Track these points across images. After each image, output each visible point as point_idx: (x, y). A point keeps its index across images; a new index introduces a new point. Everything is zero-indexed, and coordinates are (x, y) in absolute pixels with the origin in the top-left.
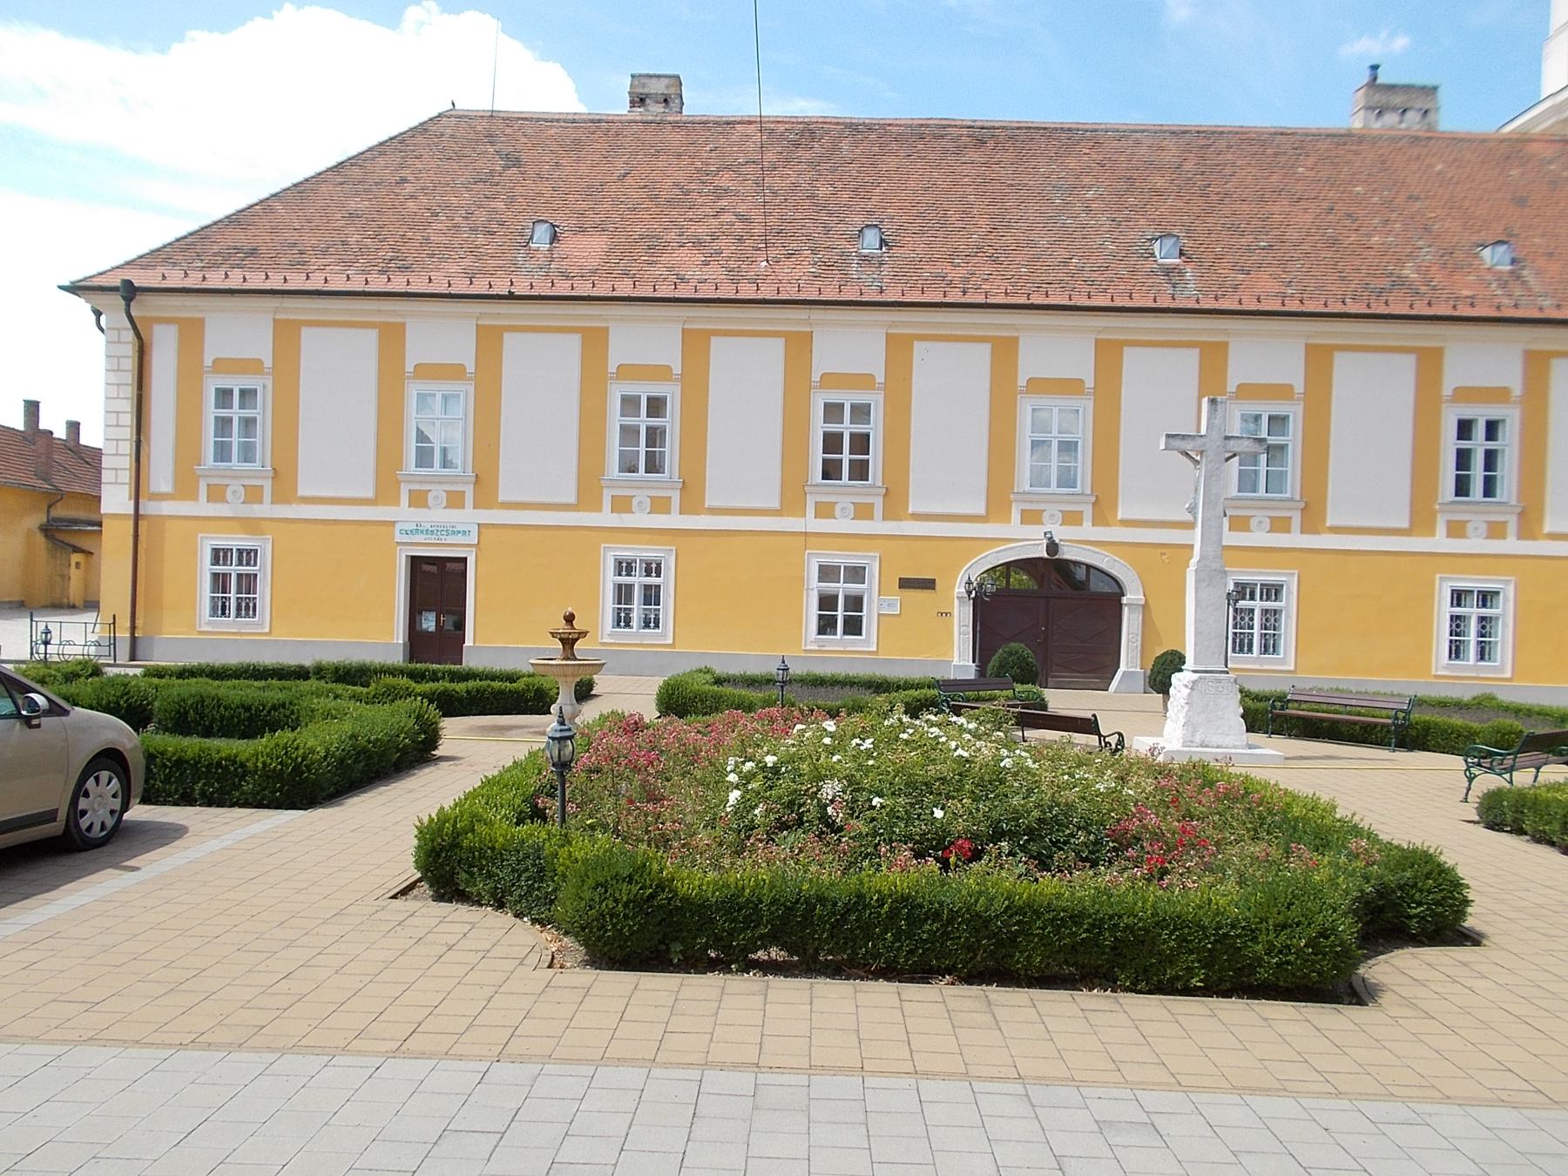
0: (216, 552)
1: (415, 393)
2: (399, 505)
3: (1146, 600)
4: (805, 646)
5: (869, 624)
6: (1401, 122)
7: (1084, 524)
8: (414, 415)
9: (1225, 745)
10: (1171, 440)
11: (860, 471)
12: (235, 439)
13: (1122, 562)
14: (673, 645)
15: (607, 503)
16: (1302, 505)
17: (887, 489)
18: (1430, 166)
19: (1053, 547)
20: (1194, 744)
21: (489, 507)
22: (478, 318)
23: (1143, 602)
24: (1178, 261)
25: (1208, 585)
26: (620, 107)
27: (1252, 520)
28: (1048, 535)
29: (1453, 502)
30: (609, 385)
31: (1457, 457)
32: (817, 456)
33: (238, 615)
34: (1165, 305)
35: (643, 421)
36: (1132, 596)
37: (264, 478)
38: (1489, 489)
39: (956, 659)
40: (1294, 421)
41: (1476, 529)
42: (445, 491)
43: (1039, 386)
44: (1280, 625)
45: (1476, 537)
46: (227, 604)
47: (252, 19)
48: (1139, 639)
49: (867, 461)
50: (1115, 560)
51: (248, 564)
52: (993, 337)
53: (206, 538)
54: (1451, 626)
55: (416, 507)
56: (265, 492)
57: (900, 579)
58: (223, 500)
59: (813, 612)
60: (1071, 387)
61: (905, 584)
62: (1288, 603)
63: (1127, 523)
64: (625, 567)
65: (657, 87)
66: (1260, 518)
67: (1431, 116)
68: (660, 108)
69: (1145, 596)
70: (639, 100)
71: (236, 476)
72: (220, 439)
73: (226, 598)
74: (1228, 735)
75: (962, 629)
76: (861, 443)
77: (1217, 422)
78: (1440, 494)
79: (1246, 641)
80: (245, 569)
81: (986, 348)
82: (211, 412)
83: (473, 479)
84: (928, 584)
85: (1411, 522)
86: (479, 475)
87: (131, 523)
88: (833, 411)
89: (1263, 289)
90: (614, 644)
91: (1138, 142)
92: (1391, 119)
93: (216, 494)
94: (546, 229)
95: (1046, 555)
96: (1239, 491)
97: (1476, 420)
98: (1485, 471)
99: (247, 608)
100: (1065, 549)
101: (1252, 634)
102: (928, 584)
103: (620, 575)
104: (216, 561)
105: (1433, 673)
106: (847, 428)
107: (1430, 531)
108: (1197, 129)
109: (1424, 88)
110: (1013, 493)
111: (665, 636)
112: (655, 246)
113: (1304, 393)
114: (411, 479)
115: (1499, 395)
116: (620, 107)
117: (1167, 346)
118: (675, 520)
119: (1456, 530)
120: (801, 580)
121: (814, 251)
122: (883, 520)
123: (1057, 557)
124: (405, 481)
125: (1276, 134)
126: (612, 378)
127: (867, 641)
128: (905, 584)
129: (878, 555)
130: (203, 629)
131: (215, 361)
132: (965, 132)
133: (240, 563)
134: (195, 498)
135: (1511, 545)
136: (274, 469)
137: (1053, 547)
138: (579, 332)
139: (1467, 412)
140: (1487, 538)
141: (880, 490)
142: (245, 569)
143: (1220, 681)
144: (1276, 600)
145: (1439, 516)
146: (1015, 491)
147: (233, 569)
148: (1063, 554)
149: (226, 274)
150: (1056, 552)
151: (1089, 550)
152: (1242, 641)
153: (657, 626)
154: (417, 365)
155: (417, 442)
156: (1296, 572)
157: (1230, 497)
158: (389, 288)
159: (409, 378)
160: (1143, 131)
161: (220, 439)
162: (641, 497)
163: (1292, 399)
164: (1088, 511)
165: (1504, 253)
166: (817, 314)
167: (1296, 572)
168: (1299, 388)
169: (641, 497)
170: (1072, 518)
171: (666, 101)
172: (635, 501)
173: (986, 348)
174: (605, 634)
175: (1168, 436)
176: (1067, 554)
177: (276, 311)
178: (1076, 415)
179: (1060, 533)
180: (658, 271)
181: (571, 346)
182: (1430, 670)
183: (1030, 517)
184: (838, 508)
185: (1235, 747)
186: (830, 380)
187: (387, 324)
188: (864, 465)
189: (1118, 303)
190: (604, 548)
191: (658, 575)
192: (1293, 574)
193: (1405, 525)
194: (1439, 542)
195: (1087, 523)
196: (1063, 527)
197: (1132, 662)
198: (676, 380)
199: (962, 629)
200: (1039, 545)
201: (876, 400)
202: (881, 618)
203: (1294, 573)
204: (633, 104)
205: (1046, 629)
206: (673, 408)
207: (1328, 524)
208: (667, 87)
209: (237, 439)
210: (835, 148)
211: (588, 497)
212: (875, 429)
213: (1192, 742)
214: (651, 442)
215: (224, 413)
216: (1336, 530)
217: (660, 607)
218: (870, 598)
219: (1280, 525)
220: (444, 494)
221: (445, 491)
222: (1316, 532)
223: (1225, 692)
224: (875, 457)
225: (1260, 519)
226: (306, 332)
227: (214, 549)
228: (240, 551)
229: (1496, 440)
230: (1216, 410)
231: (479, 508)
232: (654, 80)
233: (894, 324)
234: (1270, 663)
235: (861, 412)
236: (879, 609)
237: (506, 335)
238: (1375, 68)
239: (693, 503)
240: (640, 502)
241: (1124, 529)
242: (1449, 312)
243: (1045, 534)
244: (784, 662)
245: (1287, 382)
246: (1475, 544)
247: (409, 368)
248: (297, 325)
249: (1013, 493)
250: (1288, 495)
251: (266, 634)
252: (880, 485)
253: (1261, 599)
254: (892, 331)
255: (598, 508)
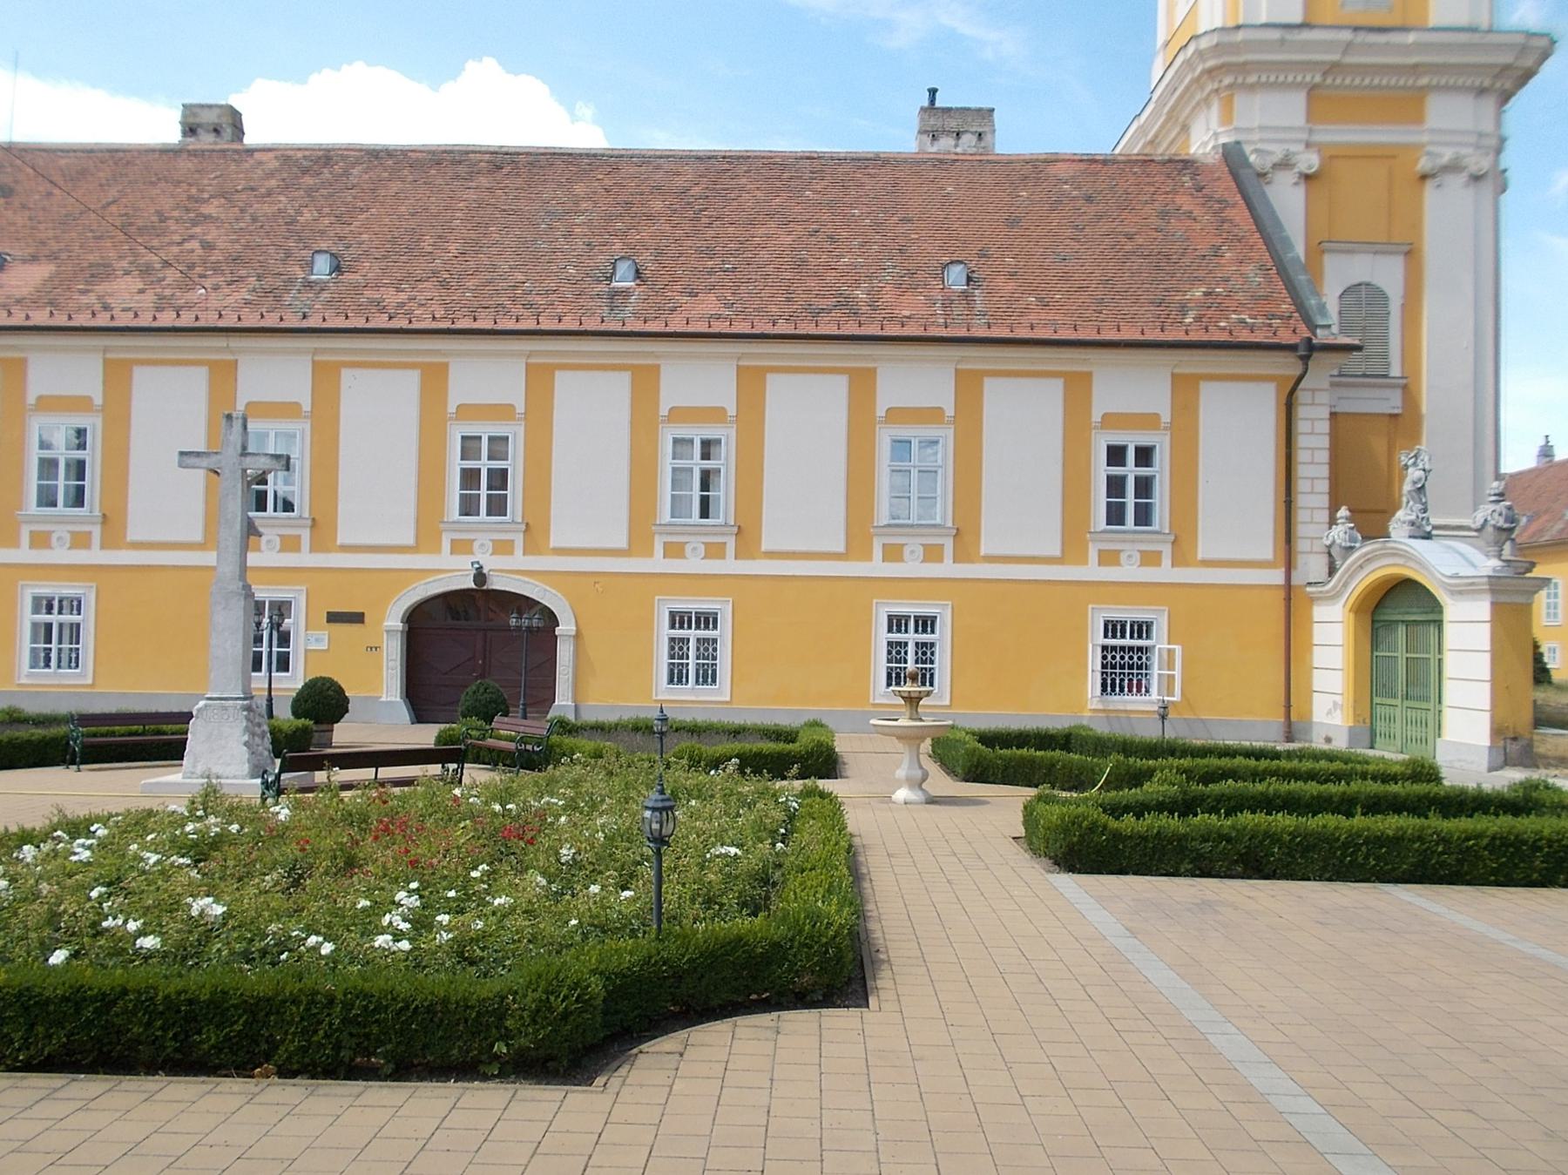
0: (37, 600)
1: (888, 440)
2: (1086, 563)
3: (578, 631)
4: (656, 695)
5: (297, 660)
6: (956, 146)
7: (945, 561)
8: (888, 462)
9: (225, 775)
10: (185, 458)
11: (498, 506)
12: (1130, 500)
13: (554, 591)
14: (92, 686)
15: (446, 546)
16: (1172, 538)
17: (958, 529)
18: (942, 188)
19: (480, 577)
20: (195, 776)
21: (971, 561)
22: (314, 354)
23: (574, 633)
24: (632, 283)
25: (224, 608)
26: (171, 135)
27: (1122, 554)
28: (476, 566)
29: (889, 526)
30: (877, 429)
31: (1064, 486)
32: (454, 491)
33: (697, 682)
34: (211, 324)
35: (1130, 470)
36: (565, 628)
37: (93, 523)
38: (1144, 516)
39: (384, 696)
40: (1161, 453)
41: (912, 552)
42: (923, 545)
43: (897, 415)
44: (1152, 664)
45: (913, 560)
46: (684, 671)
47: (350, 63)
48: (571, 670)
49: (84, 486)
50: (545, 590)
51: (899, 631)
52: (423, 363)
53: (27, 585)
54: (688, 649)
55: (1105, 565)
56: (302, 542)
57: (328, 613)
58: (1117, 563)
59: (25, 644)
60: (932, 415)
61: (334, 618)
62: (723, 632)
63: (771, 555)
64: (897, 623)
65: (209, 118)
66: (696, 544)
67: (987, 138)
68: (211, 138)
69: (577, 625)
70: (190, 130)
71: (61, 521)
72: (46, 482)
73: (682, 664)
74: (229, 765)
75: (390, 664)
76: (499, 479)
77: (231, 438)
78: (1092, 525)
79: (1109, 682)
80: (703, 633)
81: (626, 377)
82: (1101, 471)
83: (100, 520)
84: (357, 618)
85: (1063, 551)
86: (317, 518)
87: (1282, 594)
88: (469, 446)
89: (702, 311)
90: (32, 685)
91: (658, 167)
92: (946, 143)
93: (893, 554)
94: (629, 266)
95: (474, 587)
96: (672, 517)
97: (1155, 446)
98: (702, 491)
99: (707, 676)
100: (495, 579)
101: (50, 649)
102: (357, 618)
103: (71, 614)
104: (36, 610)
105: (871, 701)
106: (484, 464)
107: (1082, 560)
108: (723, 154)
109: (979, 110)
110: (1090, 532)
111: (941, 697)
112: (102, 272)
113: (525, 414)
114: (32, 520)
115: (1149, 421)
116: (171, 135)
117: (181, 364)
118: (96, 556)
119: (1108, 558)
120: (648, 624)
121: (259, 277)
122: (311, 552)
123: (485, 588)
124: (660, 534)
125: (802, 158)
126: (663, 422)
127: (293, 678)
128: (334, 618)
129: (304, 588)
130: (877, 701)
131: (1105, 416)
132: (487, 157)
133: (698, 627)
134: (650, 554)
135: (730, 565)
136: (314, 519)
137: (480, 577)
138: (1061, 377)
139: (1117, 439)
140: (1141, 565)
141: (304, 521)
142: (703, 633)
143: (225, 708)
144: (1147, 638)
145: (875, 540)
146: (875, 524)
147: (693, 634)
148: (492, 584)
149: (51, 312)
150: (484, 583)
151: (519, 580)
152: (680, 672)
153: (714, 681)
154: (889, 409)
155: (40, 478)
156: (950, 603)
157: (451, 520)
158: (178, 324)
159: (451, 419)
160: (669, 157)
161: (46, 482)
162: (61, 532)
163: (514, 419)
164: (519, 539)
165: (960, 272)
166: (236, 342)
167: (950, 603)
168: (1166, 417)
169: (61, 532)
170: (503, 548)
171: (216, 130)
172: (54, 537)
173: (626, 377)
174: (22, 676)
175: (182, 453)
176: (497, 583)
177: (106, 350)
178: (45, 437)
179: (490, 563)
180: (91, 299)
181: (410, 381)
182: (869, 699)
183: (460, 547)
184: (907, 550)
185: (235, 777)
186: (466, 412)
187: (430, 364)
188: (80, 491)
189: (545, 326)
190: (22, 586)
191: (715, 627)
192: (92, 587)
193: (841, 548)
194: (1092, 571)
195: (519, 551)
196: (493, 557)
197: (563, 695)
198: (1165, 429)
199: (390, 664)
200: (467, 575)
201: (516, 433)
202: (309, 654)
203: (1164, 610)
204: (185, 134)
205: (484, 662)
206: (1162, 459)
207: (763, 549)
208: (219, 117)
209: (58, 483)
210: (346, 174)
211: (639, 542)
212: (515, 466)
213: (193, 773)
214: (705, 486)
215: (1117, 471)
216: (771, 555)
217: (290, 650)
218: (297, 633)
219: (715, 551)
220: (278, 539)
221: (923, 545)
222: (327, 550)
223: (231, 719)
224: (92, 483)
225: (1129, 553)
226: (346, 374)
227: (889, 616)
228: (917, 619)
229: (1151, 466)
230: (232, 426)
231: (959, 562)
232: (206, 111)
233: (962, 360)
234: (706, 693)
235: (499, 446)
236: (306, 645)
237: (557, 373)
238: (933, 92)
239: (1182, 556)
240: (482, 545)
241: (987, 565)
242: (1094, 336)
243: (472, 564)
244: (662, 712)
245: (86, 394)
246: (1129, 571)
247: (452, 409)
248: (128, 365)
249: (1090, 532)
250: (721, 521)
251: (727, 703)
252: (1167, 531)
253: (916, 631)
254: (532, 360)
255: (867, 556)
